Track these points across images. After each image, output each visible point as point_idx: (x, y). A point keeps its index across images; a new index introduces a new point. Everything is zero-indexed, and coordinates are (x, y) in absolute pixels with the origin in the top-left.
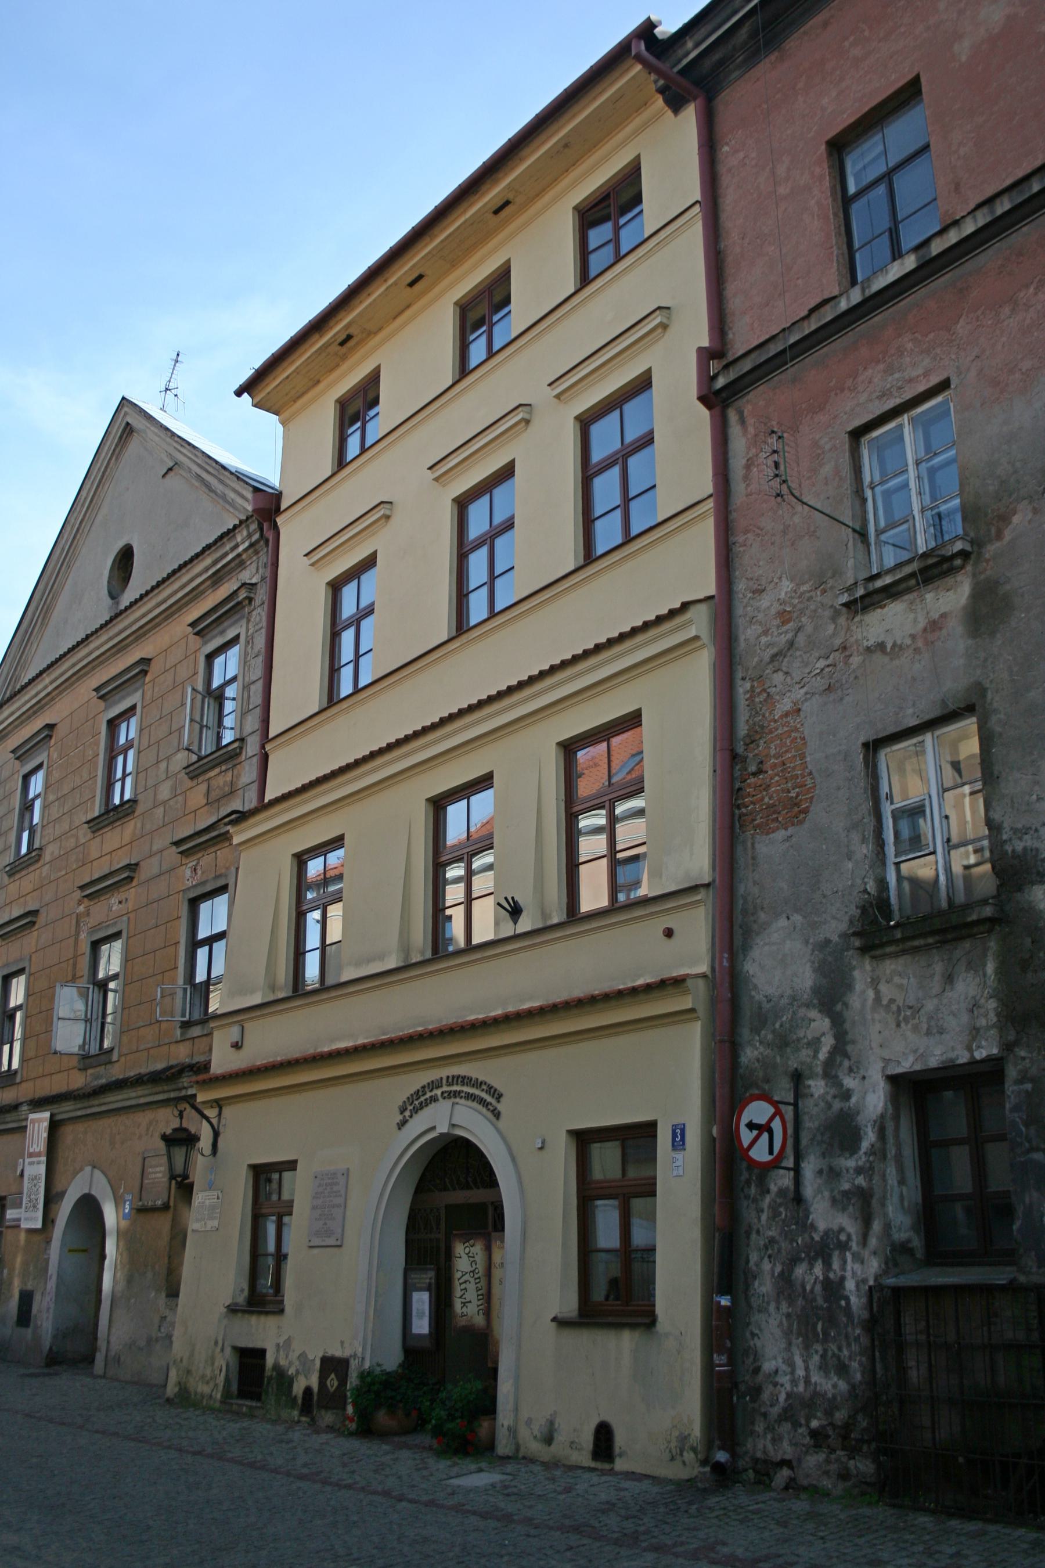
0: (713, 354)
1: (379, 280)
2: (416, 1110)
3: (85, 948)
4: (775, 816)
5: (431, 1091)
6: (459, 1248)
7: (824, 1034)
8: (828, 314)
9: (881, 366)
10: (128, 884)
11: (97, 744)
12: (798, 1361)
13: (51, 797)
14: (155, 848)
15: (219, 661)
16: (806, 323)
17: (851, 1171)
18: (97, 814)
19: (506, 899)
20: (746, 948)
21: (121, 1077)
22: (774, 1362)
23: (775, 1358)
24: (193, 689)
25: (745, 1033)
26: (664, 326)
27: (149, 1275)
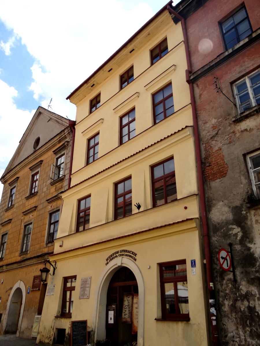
0: (189, 72)
1: (124, 49)
2: (111, 260)
3: (23, 227)
4: (216, 176)
5: (116, 254)
6: (126, 299)
7: (239, 232)
8: (222, 57)
9: (239, 66)
10: (35, 211)
11: (29, 180)
12: (241, 333)
13: (17, 193)
14: (42, 202)
15: (59, 159)
16: (216, 60)
17: (254, 272)
18: (28, 195)
19: (137, 203)
20: (210, 211)
21: (30, 257)
22: (232, 334)
23: (232, 332)
24: (53, 165)
25: (212, 233)
26: (175, 70)
27: (33, 308)
